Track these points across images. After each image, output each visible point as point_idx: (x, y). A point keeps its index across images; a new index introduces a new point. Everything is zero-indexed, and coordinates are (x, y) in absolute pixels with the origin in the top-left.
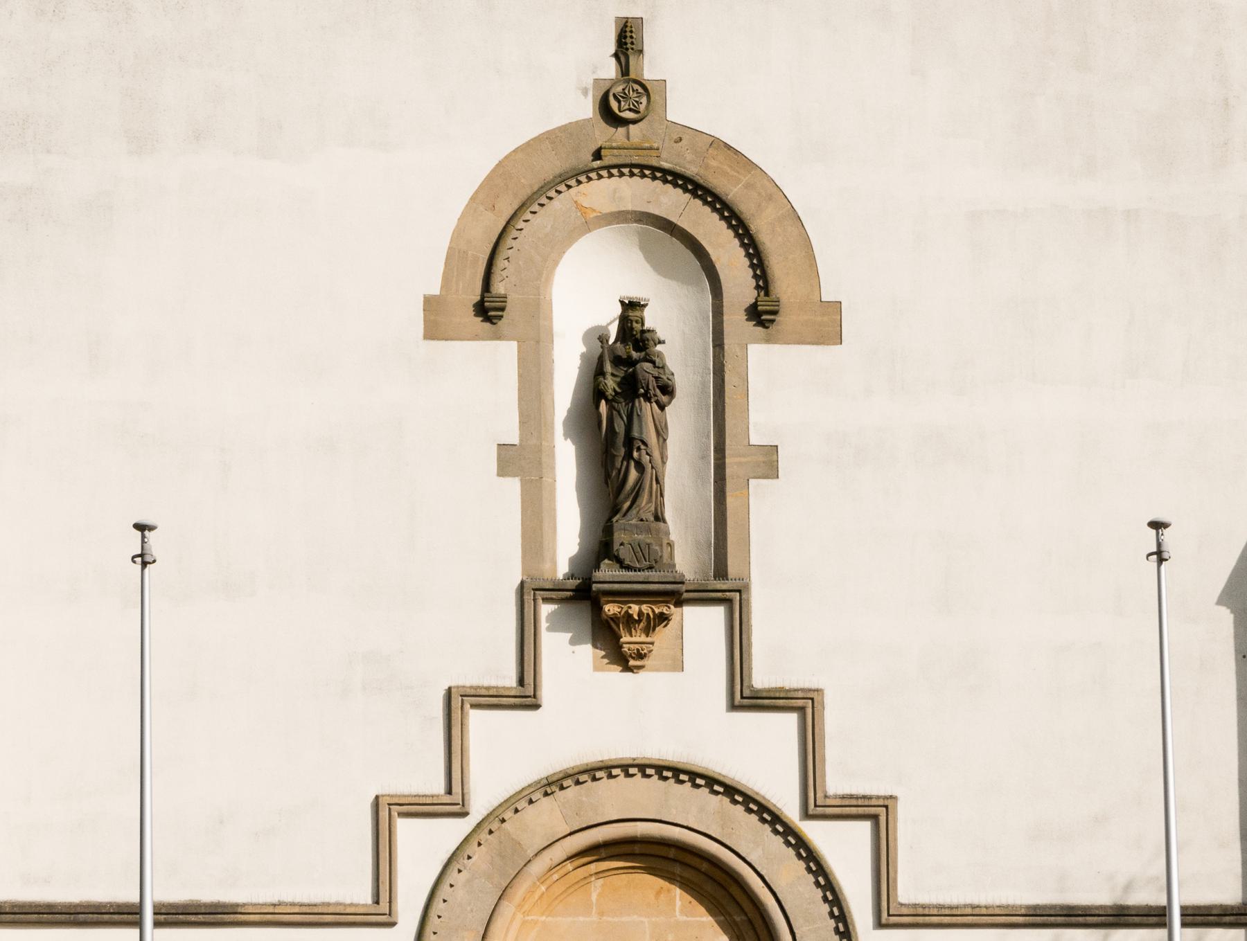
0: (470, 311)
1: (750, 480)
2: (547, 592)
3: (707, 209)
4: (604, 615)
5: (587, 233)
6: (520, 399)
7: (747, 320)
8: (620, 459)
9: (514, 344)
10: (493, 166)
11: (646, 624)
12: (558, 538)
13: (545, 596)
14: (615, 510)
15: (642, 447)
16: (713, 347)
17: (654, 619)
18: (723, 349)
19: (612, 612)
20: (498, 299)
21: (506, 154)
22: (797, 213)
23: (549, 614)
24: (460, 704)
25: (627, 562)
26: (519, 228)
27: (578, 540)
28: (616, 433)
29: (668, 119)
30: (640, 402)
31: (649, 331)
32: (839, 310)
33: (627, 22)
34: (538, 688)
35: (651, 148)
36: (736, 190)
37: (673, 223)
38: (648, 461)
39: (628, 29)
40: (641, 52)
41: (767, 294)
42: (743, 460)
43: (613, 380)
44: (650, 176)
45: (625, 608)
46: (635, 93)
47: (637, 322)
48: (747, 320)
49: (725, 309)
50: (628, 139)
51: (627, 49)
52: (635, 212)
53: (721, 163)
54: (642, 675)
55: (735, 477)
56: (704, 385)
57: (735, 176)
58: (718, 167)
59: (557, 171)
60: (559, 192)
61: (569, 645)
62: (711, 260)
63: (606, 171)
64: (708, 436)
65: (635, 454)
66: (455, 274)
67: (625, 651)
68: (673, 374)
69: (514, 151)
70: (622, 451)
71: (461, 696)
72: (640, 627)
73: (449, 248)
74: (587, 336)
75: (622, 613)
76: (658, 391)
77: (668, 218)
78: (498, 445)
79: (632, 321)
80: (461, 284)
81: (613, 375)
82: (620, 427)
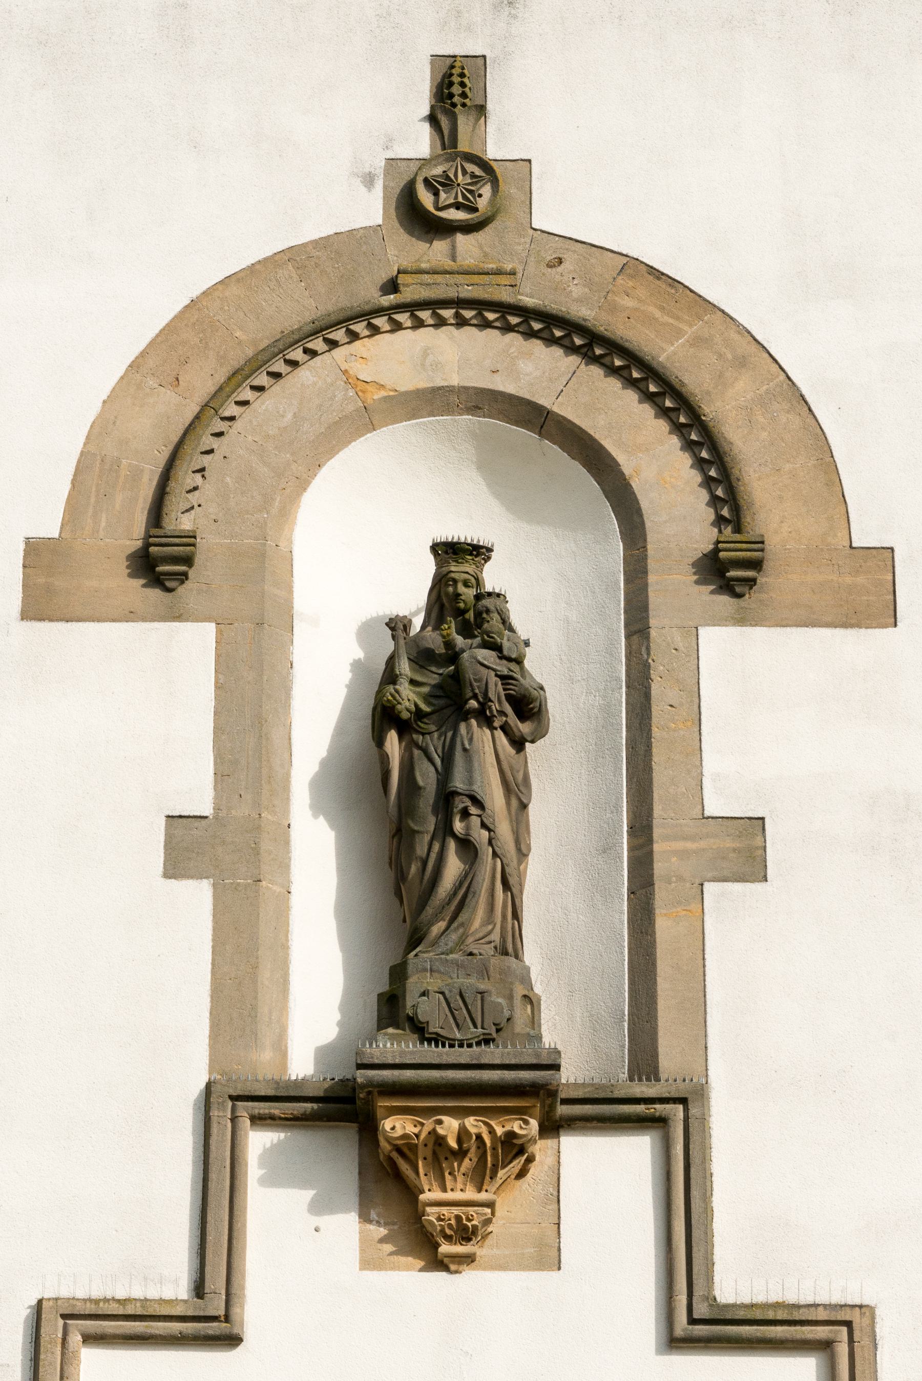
0: (122, 567)
1: (708, 886)
2: (262, 1104)
3: (614, 384)
4: (383, 1143)
5: (369, 431)
6: (218, 730)
7: (697, 582)
8: (427, 838)
9: (209, 630)
10: (179, 307)
11: (475, 1160)
12: (291, 1004)
13: (256, 1111)
14: (415, 939)
15: (473, 810)
16: (628, 637)
17: (494, 1149)
18: (647, 637)
19: (399, 1132)
20: (177, 540)
21: (205, 288)
22: (798, 389)
23: (266, 1151)
24: (60, 1335)
25: (434, 1028)
26: (227, 414)
27: (337, 1016)
28: (420, 788)
29: (533, 226)
30: (469, 728)
31: (490, 594)
32: (890, 563)
33: (452, 67)
34: (235, 1300)
35: (499, 272)
36: (672, 348)
37: (546, 408)
38: (487, 841)
39: (456, 71)
40: (481, 110)
41: (738, 529)
42: (690, 845)
43: (414, 692)
44: (497, 324)
45: (429, 1124)
46: (468, 176)
47: (466, 584)
48: (697, 582)
49: (651, 564)
50: (454, 259)
51: (454, 105)
52: (466, 388)
53: (640, 301)
54: (469, 1277)
55: (674, 879)
56: (608, 710)
57: (672, 324)
58: (636, 309)
59: (308, 316)
60: (312, 353)
61: (307, 1215)
62: (623, 474)
63: (408, 314)
64: (617, 808)
65: (458, 826)
66: (93, 500)
67: (430, 1222)
68: (542, 688)
69: (221, 282)
70: (431, 823)
71: (64, 1317)
72: (463, 1169)
73: (82, 453)
74: (365, 631)
75: (422, 1136)
76: (508, 709)
77: (534, 399)
78: (168, 817)
79: (455, 581)
80: (104, 519)
81: (413, 682)
82: (426, 776)
